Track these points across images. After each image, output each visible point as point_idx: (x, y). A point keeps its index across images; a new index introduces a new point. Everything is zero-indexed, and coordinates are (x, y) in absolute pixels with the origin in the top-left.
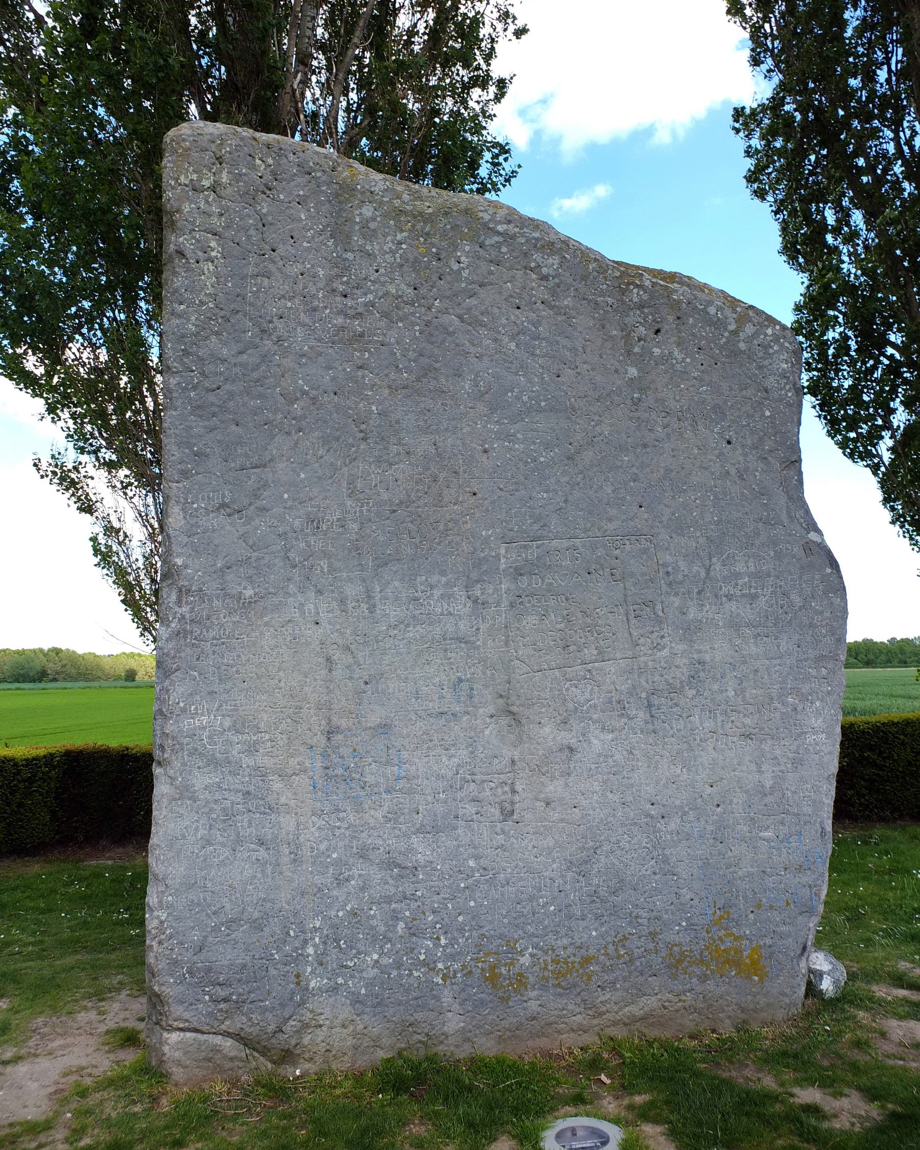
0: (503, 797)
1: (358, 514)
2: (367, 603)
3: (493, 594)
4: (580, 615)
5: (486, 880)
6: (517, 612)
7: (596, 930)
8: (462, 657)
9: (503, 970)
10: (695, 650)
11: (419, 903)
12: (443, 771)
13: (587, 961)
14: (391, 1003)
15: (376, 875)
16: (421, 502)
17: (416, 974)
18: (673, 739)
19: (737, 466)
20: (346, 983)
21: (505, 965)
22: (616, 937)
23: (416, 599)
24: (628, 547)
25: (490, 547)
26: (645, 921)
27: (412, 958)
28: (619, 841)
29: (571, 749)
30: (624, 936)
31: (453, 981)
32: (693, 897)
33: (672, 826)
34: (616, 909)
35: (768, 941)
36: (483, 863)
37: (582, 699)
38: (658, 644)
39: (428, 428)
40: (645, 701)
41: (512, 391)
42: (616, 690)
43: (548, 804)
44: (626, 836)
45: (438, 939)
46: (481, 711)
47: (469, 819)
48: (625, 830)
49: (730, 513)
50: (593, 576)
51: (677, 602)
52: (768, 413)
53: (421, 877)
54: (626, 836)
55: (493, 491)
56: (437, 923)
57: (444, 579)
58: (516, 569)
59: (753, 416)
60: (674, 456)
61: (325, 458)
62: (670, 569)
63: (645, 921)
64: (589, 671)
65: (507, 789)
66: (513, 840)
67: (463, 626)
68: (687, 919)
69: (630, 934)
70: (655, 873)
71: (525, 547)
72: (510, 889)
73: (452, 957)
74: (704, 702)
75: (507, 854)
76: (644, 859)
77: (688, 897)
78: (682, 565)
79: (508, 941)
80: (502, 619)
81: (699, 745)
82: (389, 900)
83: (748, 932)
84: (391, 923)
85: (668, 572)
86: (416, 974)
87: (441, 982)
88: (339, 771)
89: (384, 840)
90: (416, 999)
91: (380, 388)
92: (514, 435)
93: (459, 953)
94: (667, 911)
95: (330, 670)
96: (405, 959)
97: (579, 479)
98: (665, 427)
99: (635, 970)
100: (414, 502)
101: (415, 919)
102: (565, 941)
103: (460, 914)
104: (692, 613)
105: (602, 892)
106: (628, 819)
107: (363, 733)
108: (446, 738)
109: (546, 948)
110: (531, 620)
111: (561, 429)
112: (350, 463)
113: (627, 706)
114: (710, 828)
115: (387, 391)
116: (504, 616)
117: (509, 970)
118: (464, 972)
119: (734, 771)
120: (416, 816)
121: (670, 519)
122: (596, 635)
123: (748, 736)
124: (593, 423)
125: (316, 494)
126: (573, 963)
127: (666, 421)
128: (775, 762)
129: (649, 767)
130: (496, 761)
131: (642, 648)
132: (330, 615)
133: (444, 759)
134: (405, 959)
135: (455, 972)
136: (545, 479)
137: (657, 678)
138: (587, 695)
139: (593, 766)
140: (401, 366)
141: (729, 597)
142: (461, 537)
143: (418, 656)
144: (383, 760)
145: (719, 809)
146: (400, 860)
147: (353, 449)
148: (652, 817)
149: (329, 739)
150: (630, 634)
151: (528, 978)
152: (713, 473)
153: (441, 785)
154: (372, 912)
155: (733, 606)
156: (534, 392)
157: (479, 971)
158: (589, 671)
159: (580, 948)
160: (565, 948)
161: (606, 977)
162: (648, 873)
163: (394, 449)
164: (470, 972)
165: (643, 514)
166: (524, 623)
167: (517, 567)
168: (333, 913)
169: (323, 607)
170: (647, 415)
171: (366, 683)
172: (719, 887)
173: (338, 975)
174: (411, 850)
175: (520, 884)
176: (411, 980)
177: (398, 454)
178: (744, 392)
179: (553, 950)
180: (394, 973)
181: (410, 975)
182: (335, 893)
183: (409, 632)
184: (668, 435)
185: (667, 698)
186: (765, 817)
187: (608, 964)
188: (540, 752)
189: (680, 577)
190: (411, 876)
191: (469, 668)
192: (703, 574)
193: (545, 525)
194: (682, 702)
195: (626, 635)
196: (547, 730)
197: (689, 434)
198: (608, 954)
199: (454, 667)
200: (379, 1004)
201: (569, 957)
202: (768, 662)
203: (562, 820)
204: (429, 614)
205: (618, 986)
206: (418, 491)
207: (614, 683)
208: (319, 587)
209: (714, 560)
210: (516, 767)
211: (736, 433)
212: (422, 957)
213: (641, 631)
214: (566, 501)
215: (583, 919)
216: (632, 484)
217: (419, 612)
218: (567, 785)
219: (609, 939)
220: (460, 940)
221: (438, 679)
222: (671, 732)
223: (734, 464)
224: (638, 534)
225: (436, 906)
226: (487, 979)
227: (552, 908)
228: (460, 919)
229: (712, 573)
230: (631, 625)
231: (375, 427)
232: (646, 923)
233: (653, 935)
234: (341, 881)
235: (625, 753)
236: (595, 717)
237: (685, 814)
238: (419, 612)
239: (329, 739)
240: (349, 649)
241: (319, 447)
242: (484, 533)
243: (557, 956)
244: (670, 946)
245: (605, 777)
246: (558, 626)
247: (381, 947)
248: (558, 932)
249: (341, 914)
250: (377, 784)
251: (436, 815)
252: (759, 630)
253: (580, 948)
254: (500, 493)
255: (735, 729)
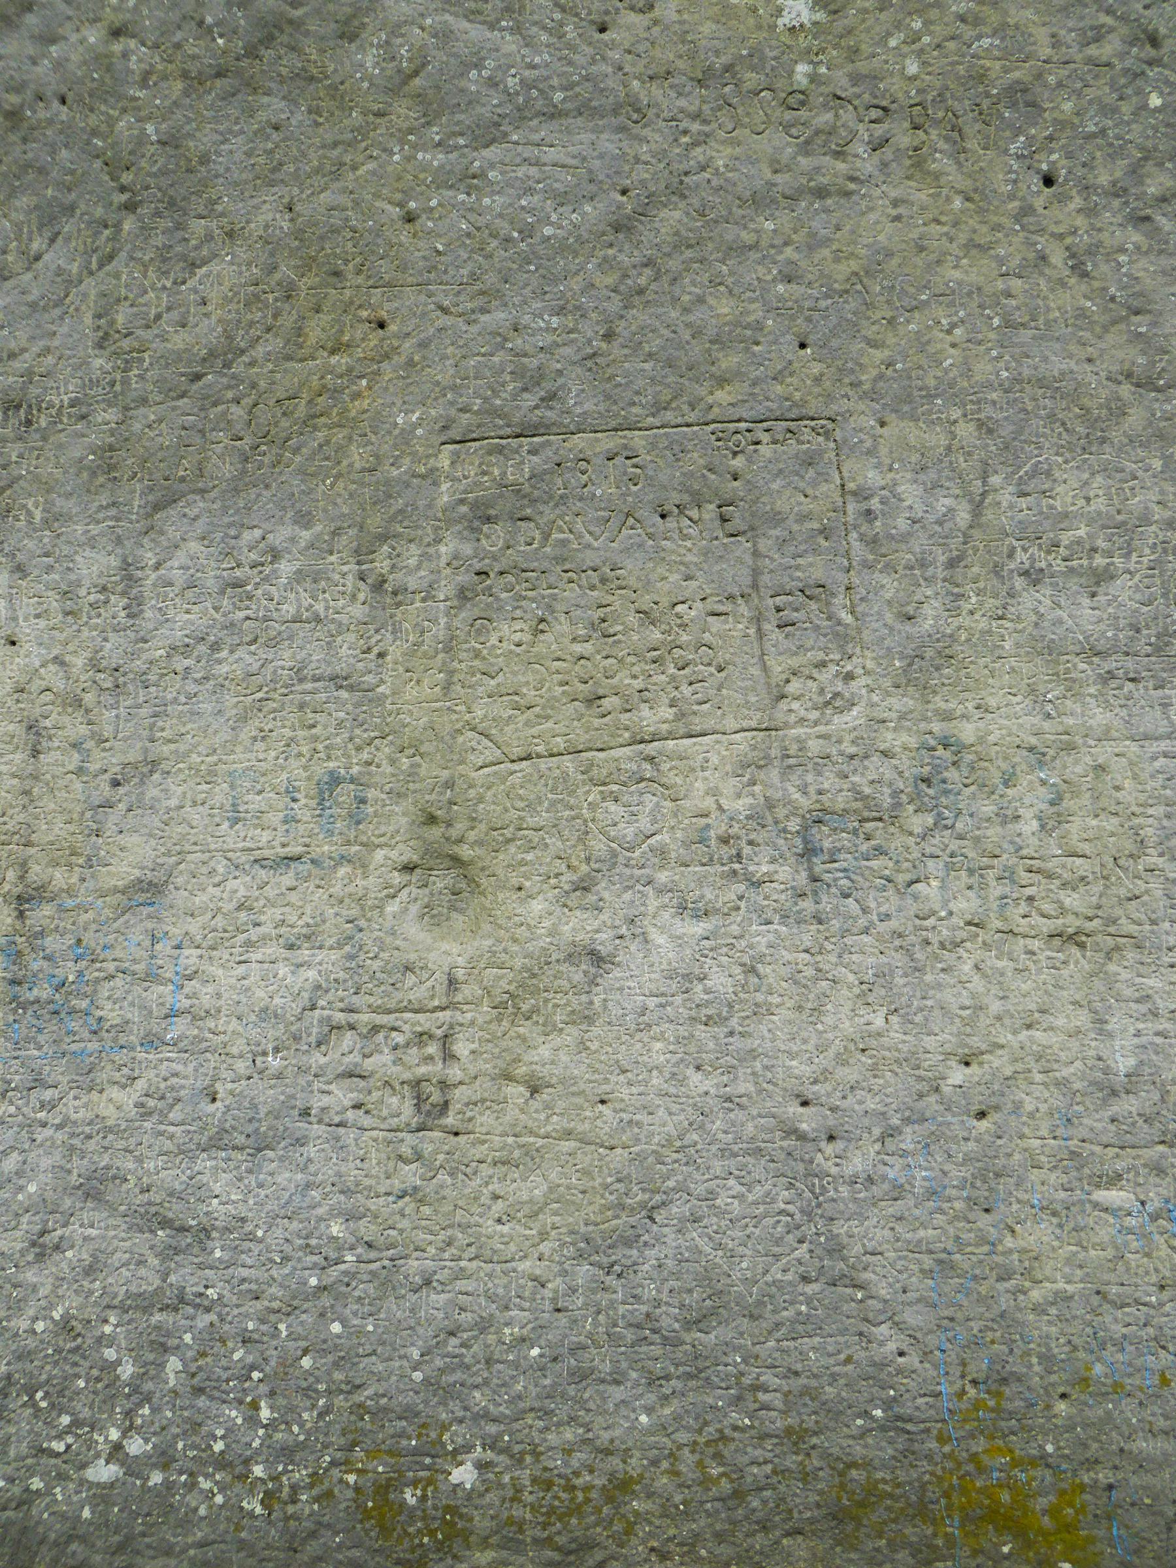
0: (423, 1070)
1: (118, 388)
2: (124, 594)
3: (419, 567)
4: (632, 619)
5: (373, 1273)
6: (477, 612)
7: (649, 1411)
8: (340, 724)
9: (410, 1497)
10: (936, 712)
11: (212, 1317)
12: (277, 1001)
13: (622, 1486)
14: (149, 1546)
15: (125, 1243)
16: (260, 351)
17: (205, 1484)
18: (865, 939)
19: (1068, 241)
20: (49, 1491)
21: (415, 1483)
22: (700, 1431)
23: (238, 584)
24: (765, 450)
25: (414, 454)
26: (776, 1399)
27: (194, 1447)
28: (711, 1196)
29: (597, 958)
30: (720, 1431)
31: (291, 1509)
32: (905, 1348)
33: (857, 1164)
34: (700, 1364)
35: (1104, 1476)
36: (368, 1230)
37: (630, 832)
38: (837, 695)
39: (274, 170)
40: (798, 841)
41: (478, 66)
42: (720, 808)
43: (534, 1091)
44: (732, 1182)
45: (255, 1406)
46: (379, 854)
47: (337, 1119)
48: (732, 1163)
49: (1045, 359)
50: (671, 523)
51: (890, 586)
52: (1155, 101)
53: (218, 1254)
54: (732, 1182)
55: (424, 314)
56: (253, 1367)
57: (306, 535)
58: (475, 505)
59: (1115, 110)
60: (897, 218)
61: (46, 257)
62: (875, 503)
63: (776, 1399)
64: (651, 759)
65: (432, 1049)
66: (443, 1177)
67: (347, 649)
68: (888, 1405)
69: (735, 1428)
70: (805, 1279)
71: (500, 450)
72: (433, 1297)
73: (288, 1453)
74: (954, 845)
75: (426, 1210)
76: (778, 1242)
77: (892, 1346)
78: (911, 493)
79: (424, 1426)
80: (439, 630)
81: (936, 958)
82: (144, 1303)
83: (1050, 1448)
84: (151, 1357)
85: (869, 512)
86: (205, 1484)
87: (259, 1510)
88: (43, 991)
89: (140, 1160)
90: (202, 1545)
91: (165, 78)
92: (481, 175)
93: (302, 1446)
94: (834, 1377)
95: (35, 753)
96: (180, 1445)
97: (642, 281)
98: (877, 146)
99: (746, 1518)
100: (243, 352)
101: (203, 1354)
102: (569, 1434)
103: (305, 1352)
104: (930, 617)
105: (668, 1320)
106: (738, 1139)
107: (99, 902)
108: (292, 919)
109: (517, 1448)
110: (509, 632)
111: (601, 156)
112: (101, 266)
113: (747, 850)
114: (957, 1174)
115: (179, 85)
116: (443, 621)
117: (424, 1498)
118: (314, 1492)
119: (1029, 1027)
120: (211, 1108)
121: (881, 376)
122: (672, 670)
123: (1075, 939)
124: (685, 139)
125: (23, 343)
126: (587, 1488)
127: (879, 130)
128: (1143, 1008)
129: (800, 1008)
130: (411, 979)
131: (795, 705)
132: (42, 623)
133: (283, 970)
134: (180, 1445)
135: (294, 1488)
136: (555, 281)
137: (829, 781)
138: (644, 823)
139: (652, 1002)
140: (209, 20)
141: (1034, 577)
142: (346, 432)
143: (243, 719)
144: (140, 968)
145: (984, 1124)
146: (174, 1210)
147: (107, 232)
148: (802, 1137)
149: (21, 915)
150: (765, 669)
151: (471, 1519)
152: (1001, 261)
153: (276, 1032)
154: (108, 1329)
155: (1043, 596)
156: (534, 67)
157: (350, 1494)
158: (651, 759)
159: (608, 1452)
160: (568, 1452)
161: (672, 1532)
162: (789, 1277)
163: (198, 226)
164: (329, 1494)
165: (810, 364)
166: (494, 640)
167: (476, 499)
168: (23, 1324)
169: (27, 605)
170: (829, 116)
171: (116, 784)
172: (976, 1326)
173: (31, 1472)
174: (202, 1193)
175: (461, 1285)
176: (192, 1500)
177: (209, 237)
178: (1093, 51)
179: (536, 1455)
180: (156, 1478)
181: (192, 1486)
182: (30, 1276)
183: (219, 662)
184: (885, 164)
185: (855, 832)
186: (1111, 1151)
187: (678, 1498)
188: (518, 963)
189: (902, 524)
190: (196, 1250)
191: (359, 749)
192: (963, 516)
193: (552, 396)
194: (897, 843)
195: (756, 671)
196: (538, 906)
197: (941, 162)
198: (677, 1474)
199: (320, 747)
200: (120, 1548)
201: (577, 1474)
202: (1134, 747)
203: (568, 1134)
204: (266, 619)
205: (703, 1552)
206: (251, 324)
207: (714, 792)
208: (20, 557)
209: (995, 480)
210: (459, 998)
211: (1069, 156)
212: (218, 1446)
213: (794, 662)
214: (608, 336)
215: (617, 1383)
216: (781, 288)
217: (241, 614)
218: (582, 1046)
219: (683, 1437)
220: (306, 1416)
221: (285, 776)
222: (862, 922)
223: (1061, 237)
224: (793, 419)
225: (251, 1326)
226: (367, 1515)
227: (535, 1352)
228: (306, 1362)
229: (989, 515)
230: (768, 645)
231: (155, 175)
232: (779, 1404)
233: (795, 1437)
234: (42, 1248)
235: (737, 970)
236: (663, 877)
237: (891, 1133)
238: (241, 614)
239: (21, 915)
240: (78, 703)
241: (31, 232)
242: (400, 420)
243: (545, 1469)
244: (844, 1466)
245: (683, 1031)
246: (578, 648)
247: (129, 1414)
248: (549, 1413)
249: (40, 1326)
250: (123, 1027)
251: (254, 1107)
252: (1111, 664)
253: (608, 1452)
254: (444, 321)
255: (1036, 920)
